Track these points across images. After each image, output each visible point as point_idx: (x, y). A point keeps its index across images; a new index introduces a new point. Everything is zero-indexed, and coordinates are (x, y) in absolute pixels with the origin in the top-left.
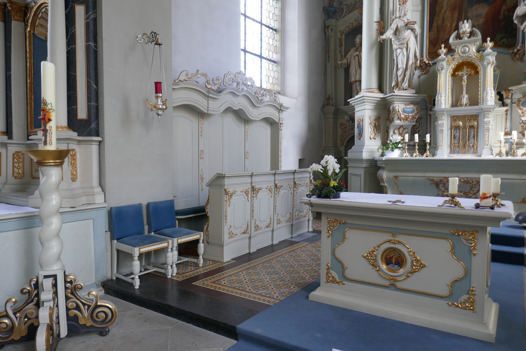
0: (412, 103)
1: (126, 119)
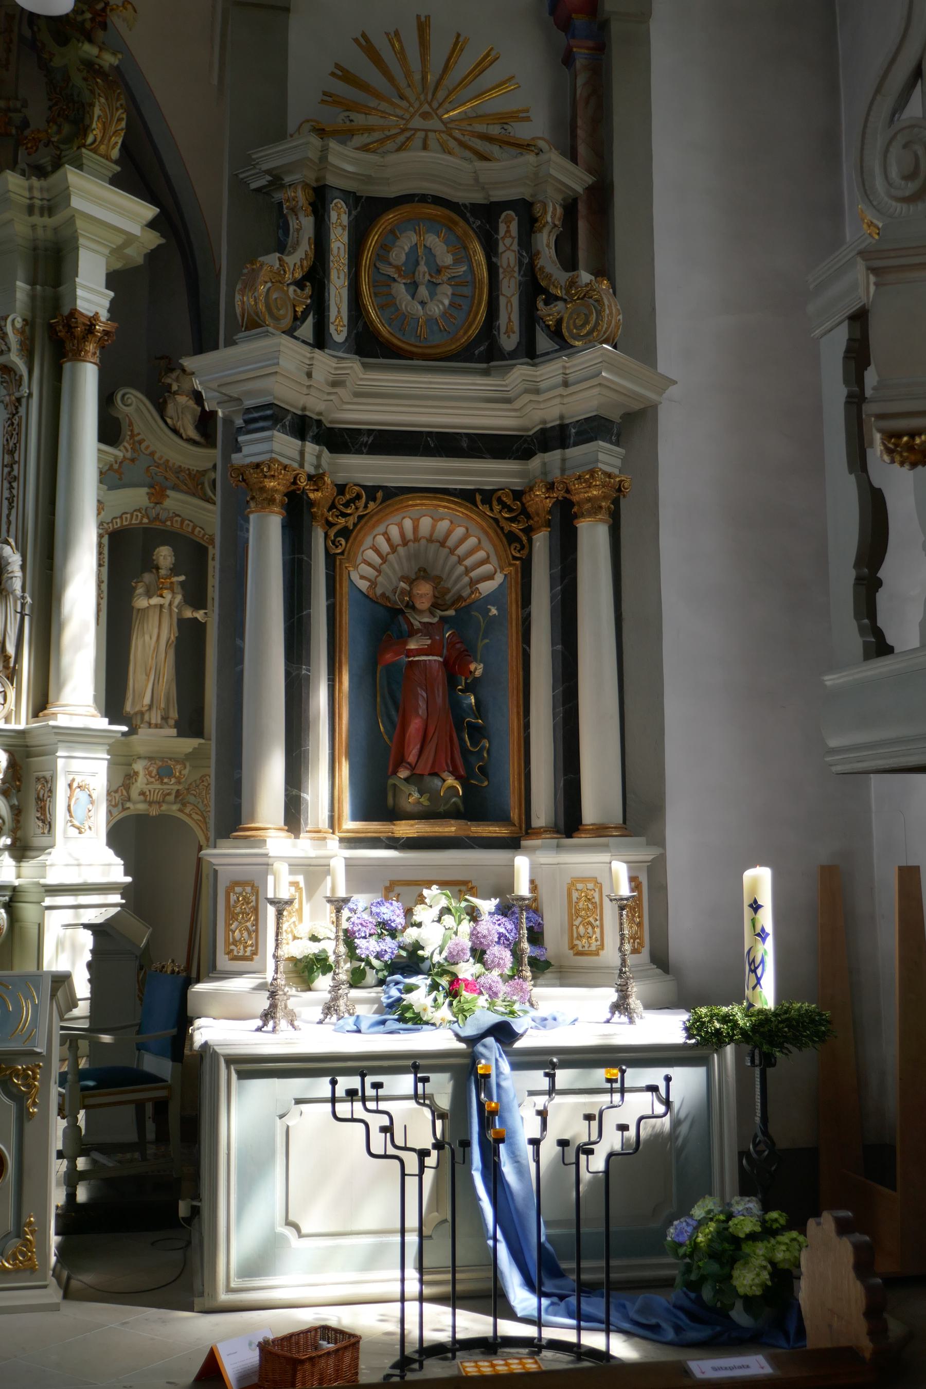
0: (356, 938)
1: (231, 916)
